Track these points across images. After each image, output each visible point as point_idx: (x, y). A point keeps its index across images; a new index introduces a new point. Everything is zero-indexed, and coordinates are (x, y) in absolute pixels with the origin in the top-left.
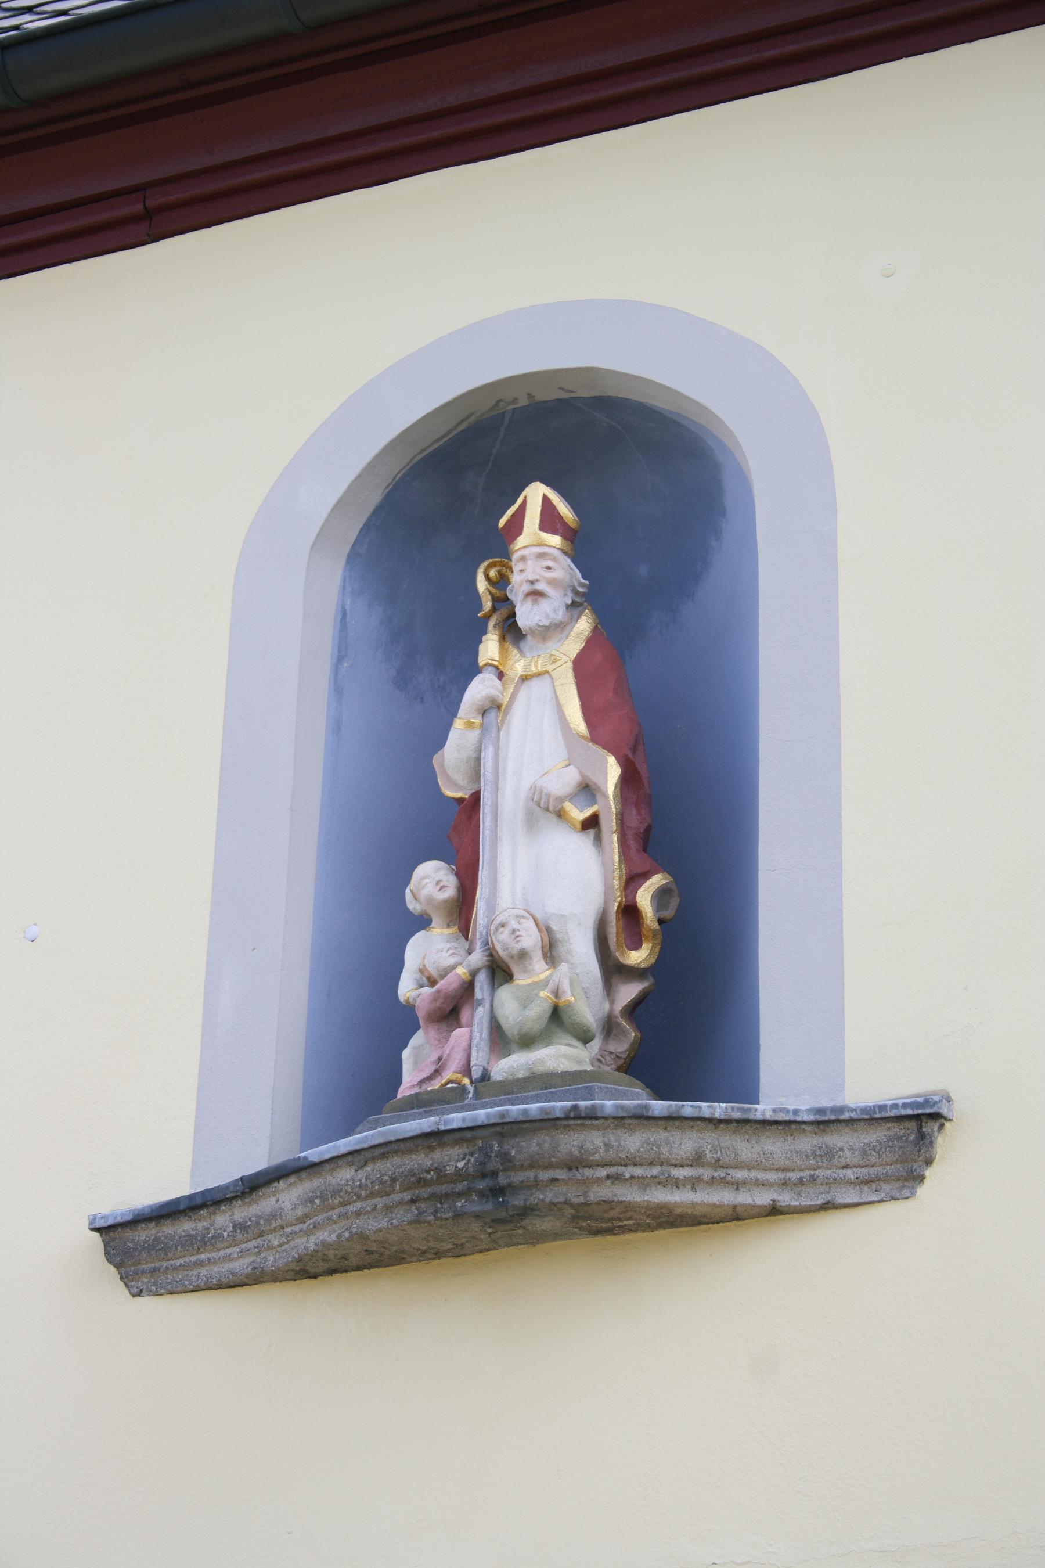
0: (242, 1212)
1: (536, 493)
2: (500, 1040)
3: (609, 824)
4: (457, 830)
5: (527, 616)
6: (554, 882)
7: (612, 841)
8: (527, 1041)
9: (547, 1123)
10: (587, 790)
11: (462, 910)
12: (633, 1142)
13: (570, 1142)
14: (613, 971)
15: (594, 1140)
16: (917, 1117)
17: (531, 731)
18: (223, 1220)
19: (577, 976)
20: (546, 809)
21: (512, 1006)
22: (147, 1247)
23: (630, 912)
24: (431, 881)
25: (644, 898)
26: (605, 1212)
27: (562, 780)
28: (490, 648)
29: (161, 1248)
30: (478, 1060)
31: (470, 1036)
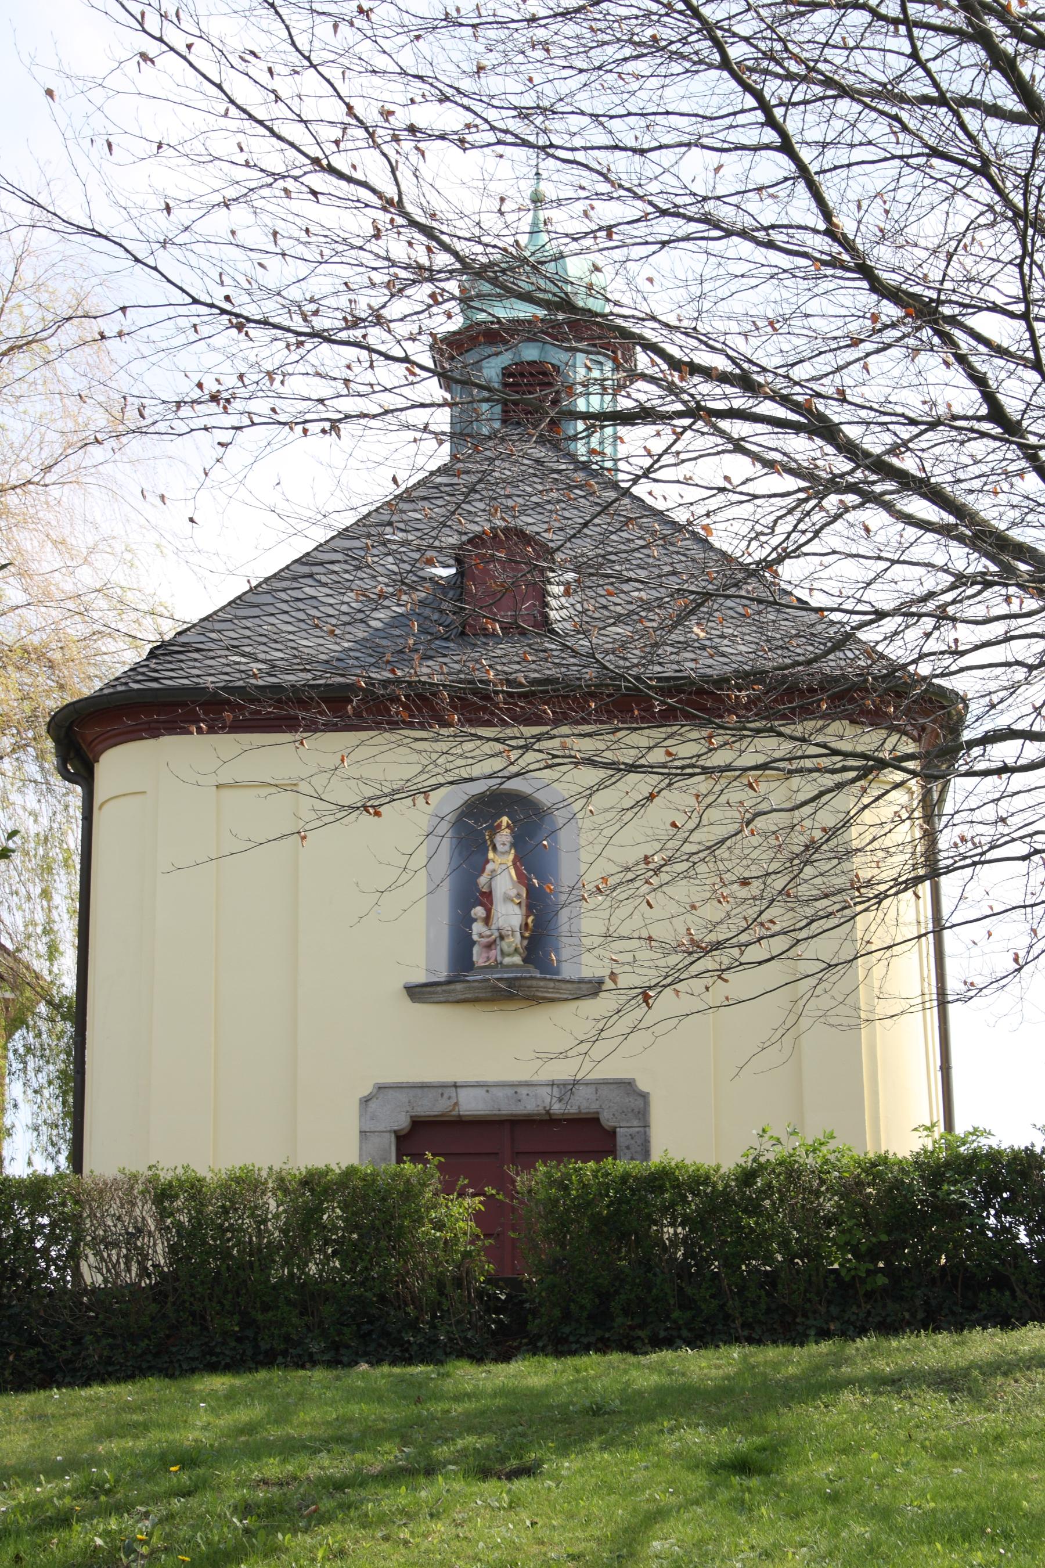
0: (444, 988)
1: (505, 820)
2: (503, 954)
3: (524, 904)
4: (486, 899)
5: (499, 847)
6: (509, 915)
7: (524, 908)
8: (509, 955)
9: (526, 978)
10: (518, 895)
11: (487, 920)
12: (542, 983)
13: (529, 983)
14: (523, 937)
15: (534, 983)
16: (943, 1003)
17: (502, 875)
18: (439, 989)
19: (515, 941)
20: (508, 899)
21: (504, 945)
22: (416, 992)
23: (526, 924)
24: (479, 911)
25: (530, 920)
26: (16, 1051)
27: (513, 893)
28: (491, 855)
29: (423, 993)
30: (499, 959)
31: (494, 953)
